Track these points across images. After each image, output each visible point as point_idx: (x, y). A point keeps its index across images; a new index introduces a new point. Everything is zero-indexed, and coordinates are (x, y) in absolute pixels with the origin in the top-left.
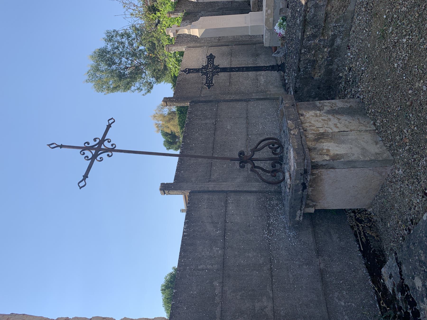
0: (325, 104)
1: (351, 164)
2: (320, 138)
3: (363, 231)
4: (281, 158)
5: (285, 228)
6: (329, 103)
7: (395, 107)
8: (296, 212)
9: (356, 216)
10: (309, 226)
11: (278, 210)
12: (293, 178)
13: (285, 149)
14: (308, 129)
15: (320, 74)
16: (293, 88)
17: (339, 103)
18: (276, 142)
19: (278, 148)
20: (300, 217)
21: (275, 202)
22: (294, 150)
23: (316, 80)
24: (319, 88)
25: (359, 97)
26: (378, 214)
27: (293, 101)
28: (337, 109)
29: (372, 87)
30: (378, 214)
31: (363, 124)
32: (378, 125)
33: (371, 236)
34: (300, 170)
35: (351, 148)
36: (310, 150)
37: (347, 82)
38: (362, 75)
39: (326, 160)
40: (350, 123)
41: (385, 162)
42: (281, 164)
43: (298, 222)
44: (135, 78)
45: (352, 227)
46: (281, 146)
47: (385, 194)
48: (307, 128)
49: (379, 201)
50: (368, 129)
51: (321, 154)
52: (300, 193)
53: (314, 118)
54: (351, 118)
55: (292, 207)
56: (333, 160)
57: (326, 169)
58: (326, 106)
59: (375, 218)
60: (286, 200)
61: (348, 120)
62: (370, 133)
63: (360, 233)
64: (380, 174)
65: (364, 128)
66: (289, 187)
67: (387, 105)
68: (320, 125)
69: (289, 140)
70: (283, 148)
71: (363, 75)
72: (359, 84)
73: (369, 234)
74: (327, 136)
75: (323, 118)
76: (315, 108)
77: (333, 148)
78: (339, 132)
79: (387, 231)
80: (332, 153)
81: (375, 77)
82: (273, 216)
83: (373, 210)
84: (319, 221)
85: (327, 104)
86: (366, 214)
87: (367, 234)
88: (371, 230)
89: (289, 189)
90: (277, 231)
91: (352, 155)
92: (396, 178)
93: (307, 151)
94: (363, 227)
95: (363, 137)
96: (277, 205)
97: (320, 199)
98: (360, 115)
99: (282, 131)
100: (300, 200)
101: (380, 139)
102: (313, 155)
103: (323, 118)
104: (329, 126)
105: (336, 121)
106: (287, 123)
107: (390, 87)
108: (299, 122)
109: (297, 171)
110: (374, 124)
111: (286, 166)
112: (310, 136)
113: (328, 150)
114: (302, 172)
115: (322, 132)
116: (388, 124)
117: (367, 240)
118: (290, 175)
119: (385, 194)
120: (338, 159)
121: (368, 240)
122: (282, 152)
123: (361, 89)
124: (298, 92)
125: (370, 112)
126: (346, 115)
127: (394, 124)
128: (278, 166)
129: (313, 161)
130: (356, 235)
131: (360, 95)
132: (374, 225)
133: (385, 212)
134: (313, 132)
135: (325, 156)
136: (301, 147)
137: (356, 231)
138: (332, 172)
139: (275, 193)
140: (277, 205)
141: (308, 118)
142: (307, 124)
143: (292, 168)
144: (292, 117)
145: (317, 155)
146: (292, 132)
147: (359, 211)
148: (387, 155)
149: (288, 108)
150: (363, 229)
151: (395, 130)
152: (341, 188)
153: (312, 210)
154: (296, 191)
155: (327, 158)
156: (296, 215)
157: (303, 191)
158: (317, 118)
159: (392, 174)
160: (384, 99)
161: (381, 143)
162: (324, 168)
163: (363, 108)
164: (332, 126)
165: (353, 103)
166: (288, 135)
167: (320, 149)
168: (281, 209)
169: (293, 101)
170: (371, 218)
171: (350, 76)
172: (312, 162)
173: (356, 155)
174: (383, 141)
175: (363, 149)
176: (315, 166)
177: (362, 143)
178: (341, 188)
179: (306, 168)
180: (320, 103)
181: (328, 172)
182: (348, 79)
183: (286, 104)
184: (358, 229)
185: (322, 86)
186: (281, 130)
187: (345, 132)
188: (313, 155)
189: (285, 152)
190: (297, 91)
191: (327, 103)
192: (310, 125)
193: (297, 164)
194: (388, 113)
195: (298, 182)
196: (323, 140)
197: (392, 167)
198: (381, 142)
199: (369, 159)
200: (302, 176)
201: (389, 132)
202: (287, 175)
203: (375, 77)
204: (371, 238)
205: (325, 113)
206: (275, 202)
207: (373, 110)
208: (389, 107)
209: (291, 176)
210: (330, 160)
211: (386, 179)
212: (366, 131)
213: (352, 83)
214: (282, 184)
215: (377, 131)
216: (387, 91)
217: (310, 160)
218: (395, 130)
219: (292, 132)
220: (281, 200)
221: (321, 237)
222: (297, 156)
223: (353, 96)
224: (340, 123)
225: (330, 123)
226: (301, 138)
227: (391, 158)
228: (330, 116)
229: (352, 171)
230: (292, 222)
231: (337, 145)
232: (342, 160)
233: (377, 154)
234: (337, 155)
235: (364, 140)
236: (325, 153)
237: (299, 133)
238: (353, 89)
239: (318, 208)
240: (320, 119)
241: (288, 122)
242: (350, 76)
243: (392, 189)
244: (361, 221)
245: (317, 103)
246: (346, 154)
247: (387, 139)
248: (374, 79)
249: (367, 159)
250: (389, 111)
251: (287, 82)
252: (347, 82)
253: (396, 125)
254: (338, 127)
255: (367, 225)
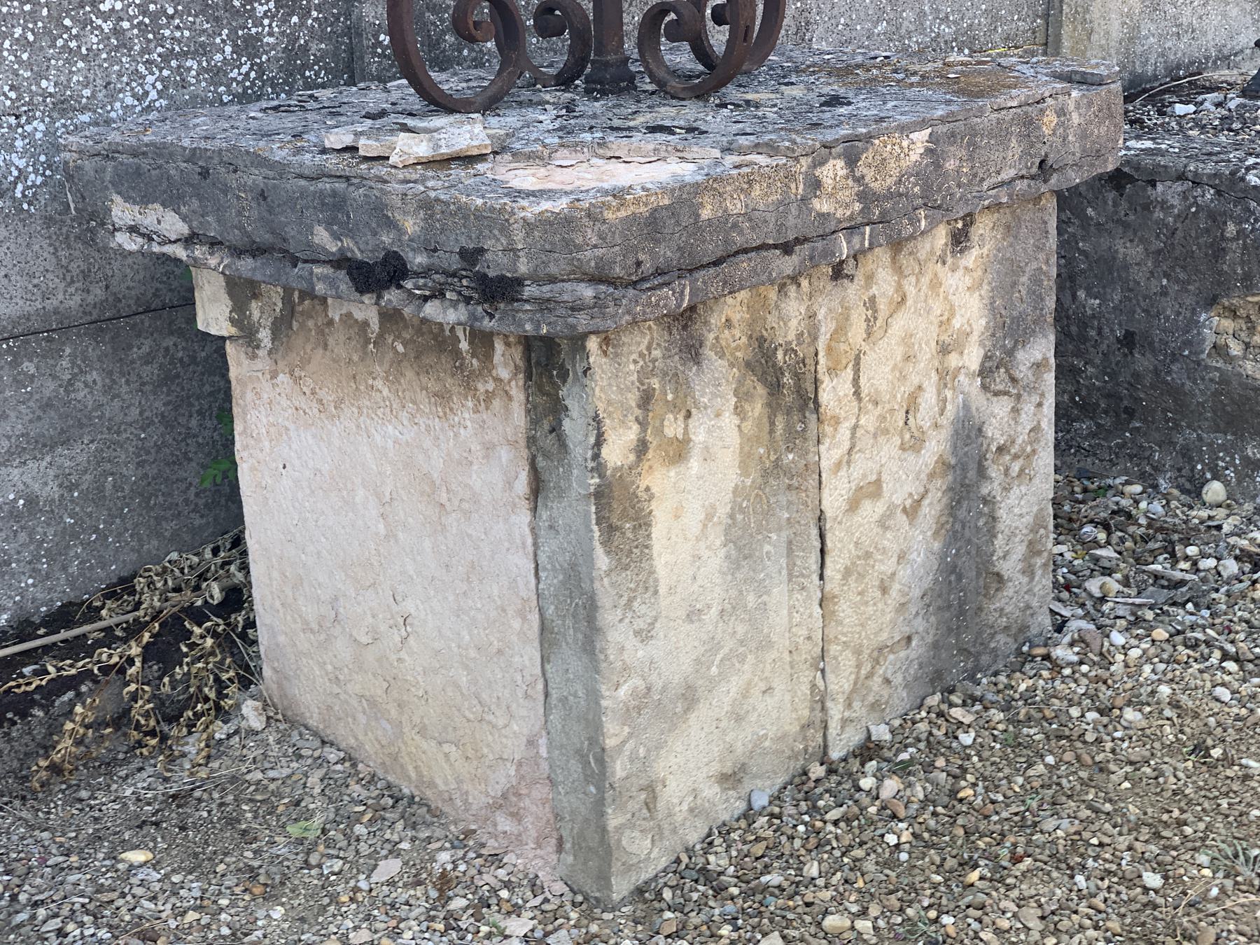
0: (1028, 408)
1: (570, 621)
2: (775, 388)
3: (86, 675)
4: (612, 82)
5: (63, 106)
6: (1036, 429)
7: (1005, 924)
8: (172, 201)
9: (199, 619)
10: (98, 292)
11: (203, 51)
12: (436, 186)
13: (690, 112)
14: (853, 291)
15: (1236, 349)
16: (1147, 161)
17: (1024, 499)
18: (748, 30)
19: (701, 51)
20: (133, 229)
21: (271, 35)
22: (684, 198)
23: (1192, 323)
24: (1129, 341)
25: (1059, 629)
26: (222, 768)
27: (1077, 165)
28: (985, 491)
29: (1144, 737)
30: (222, 768)
31: (870, 676)
32: (867, 783)
33: (54, 728)
34: (511, 250)
35: (693, 615)
36: (685, 321)
37: (1168, 539)
38: (1226, 656)
39: (599, 443)
40: (884, 590)
41: (592, 846)
42: (564, 80)
43: (94, 220)
44: (604, 93)
45: (122, 588)
46: (714, 78)
47: (360, 830)
48: (860, 279)
49: (314, 779)
50: (836, 712)
51: (646, 399)
52: (322, 237)
53: (934, 329)
54: (917, 593)
55: (204, 174)
56: (600, 495)
57: (531, 441)
58: (1015, 411)
59: (193, 746)
60: (272, 122)
61: (904, 573)
62: (805, 727)
63: (76, 648)
64: (506, 802)
65: (840, 683)
66: (368, 146)
67: (1016, 860)
68: (877, 375)
69: (771, 149)
70: (700, 94)
71: (1231, 666)
72: (1160, 634)
73: (69, 714)
74: (794, 438)
75: (929, 399)
76: (1008, 332)
77: (699, 475)
78: (821, 518)
79: (97, 838)
80: (659, 481)
81: (1216, 753)
82: (155, 17)
83: (252, 732)
84: (148, 360)
85: (1028, 420)
86: (220, 685)
87: (72, 704)
88: (98, 725)
89: (353, 149)
90: (22, 43)
91: (640, 624)
92: (478, 917)
93: (670, 298)
94: (122, 671)
95: (779, 685)
96: (249, 47)
97: (297, 380)
98: (936, 646)
99: (835, 88)
100: (262, 237)
101: (760, 801)
102: (643, 345)
103: (929, 399)
104: (864, 441)
105: (900, 490)
106: (905, 129)
107: (1153, 880)
108: (914, 221)
109: (496, 220)
110: (868, 750)
111: (547, 118)
112: (795, 306)
113: (679, 451)
114: (495, 263)
115: (825, 397)
116: (869, 866)
117: (23, 705)
118: (467, 160)
119: (360, 830)
120: (609, 530)
121: (24, 714)
122: (672, 88)
123: (1125, 649)
124: (1111, 195)
125: (957, 713)
126: (943, 556)
127: (874, 910)
128: (550, 54)
129: (593, 344)
130: (63, 617)
131: (1079, 640)
132: (140, 744)
133: (232, 822)
134: (826, 330)
135: (632, 434)
136: (711, 249)
137: (93, 614)
138: (509, 484)
139: (348, 31)
140: (249, 47)
141: (935, 284)
142: (885, 284)
143: (525, 178)
144: (950, 165)
145: (643, 374)
146: (833, 171)
147: (243, 636)
148: (644, 854)
149: (1029, 124)
150: (106, 670)
151: (831, 922)
152: (390, 536)
153: (213, 315)
154: (334, 210)
155: (616, 452)
156: (144, 200)
157: (342, 262)
158: (927, 353)
159: (507, 885)
160: (1059, 828)
161: (728, 807)
162: (534, 423)
163: (985, 659)
164: (862, 468)
165: (1023, 590)
166: (812, 139)
167: (689, 392)
168: (217, 75)
169: (1077, 165)
170: (191, 726)
171: (1210, 563)
172: (584, 336)
173: (637, 653)
174: (748, 815)
175: (690, 697)
176: (549, 364)
177: (734, 685)
178: (390, 536)
179: (529, 291)
180: (1038, 366)
181: (505, 454)
182: (1192, 551)
183: (1061, 112)
184: (109, 637)
185: (1143, 362)
186: (844, 72)
187: (814, 557)
188: (643, 345)
189: (667, 113)
190: (1119, 188)
191: (1040, 412)
192: (882, 306)
193: (565, 222)
194: (951, 863)
195: (411, 225)
196: (757, 408)
197: (559, 887)
198: (741, 806)
199: (610, 743)
200: (455, 263)
201: (812, 869)
202: (466, 133)
203: (1216, 753)
204: (39, 732)
205: (966, 406)
206: (271, 35)
207: (967, 739)
208: (997, 878)
209: (457, 172)
210: (599, 469)
211: (469, 833)
212: (820, 701)
213: (1157, 577)
214: (400, 88)
215: (817, 771)
216: (1117, 860)
217: (598, 323)
218: (831, 922)
219: (833, 171)
220: (288, 78)
221: (18, 383)
222: (633, 219)
223: (1067, 587)
224: (883, 524)
225: (889, 449)
226: (787, 248)
227: (621, 887)
228: (936, 446)
229: (516, 624)
230: (88, 165)
231: (723, 511)
232: (602, 561)
233: (651, 791)
234: (643, 522)
235: (756, 692)
236: (659, 431)
237: (827, 230)
238: (1113, 584)
239: (238, 364)
240: (923, 374)
241: (921, 137)
242: (1210, 563)
243: (391, 883)
244: (162, 654)
245: (1042, 348)
246: (649, 586)
247: (759, 849)
248: (1200, 749)
249: (613, 732)
250: (974, 876)
251: (1180, 109)
252: (1168, 539)
253: (864, 925)
254: (853, 505)
255: (134, 697)
